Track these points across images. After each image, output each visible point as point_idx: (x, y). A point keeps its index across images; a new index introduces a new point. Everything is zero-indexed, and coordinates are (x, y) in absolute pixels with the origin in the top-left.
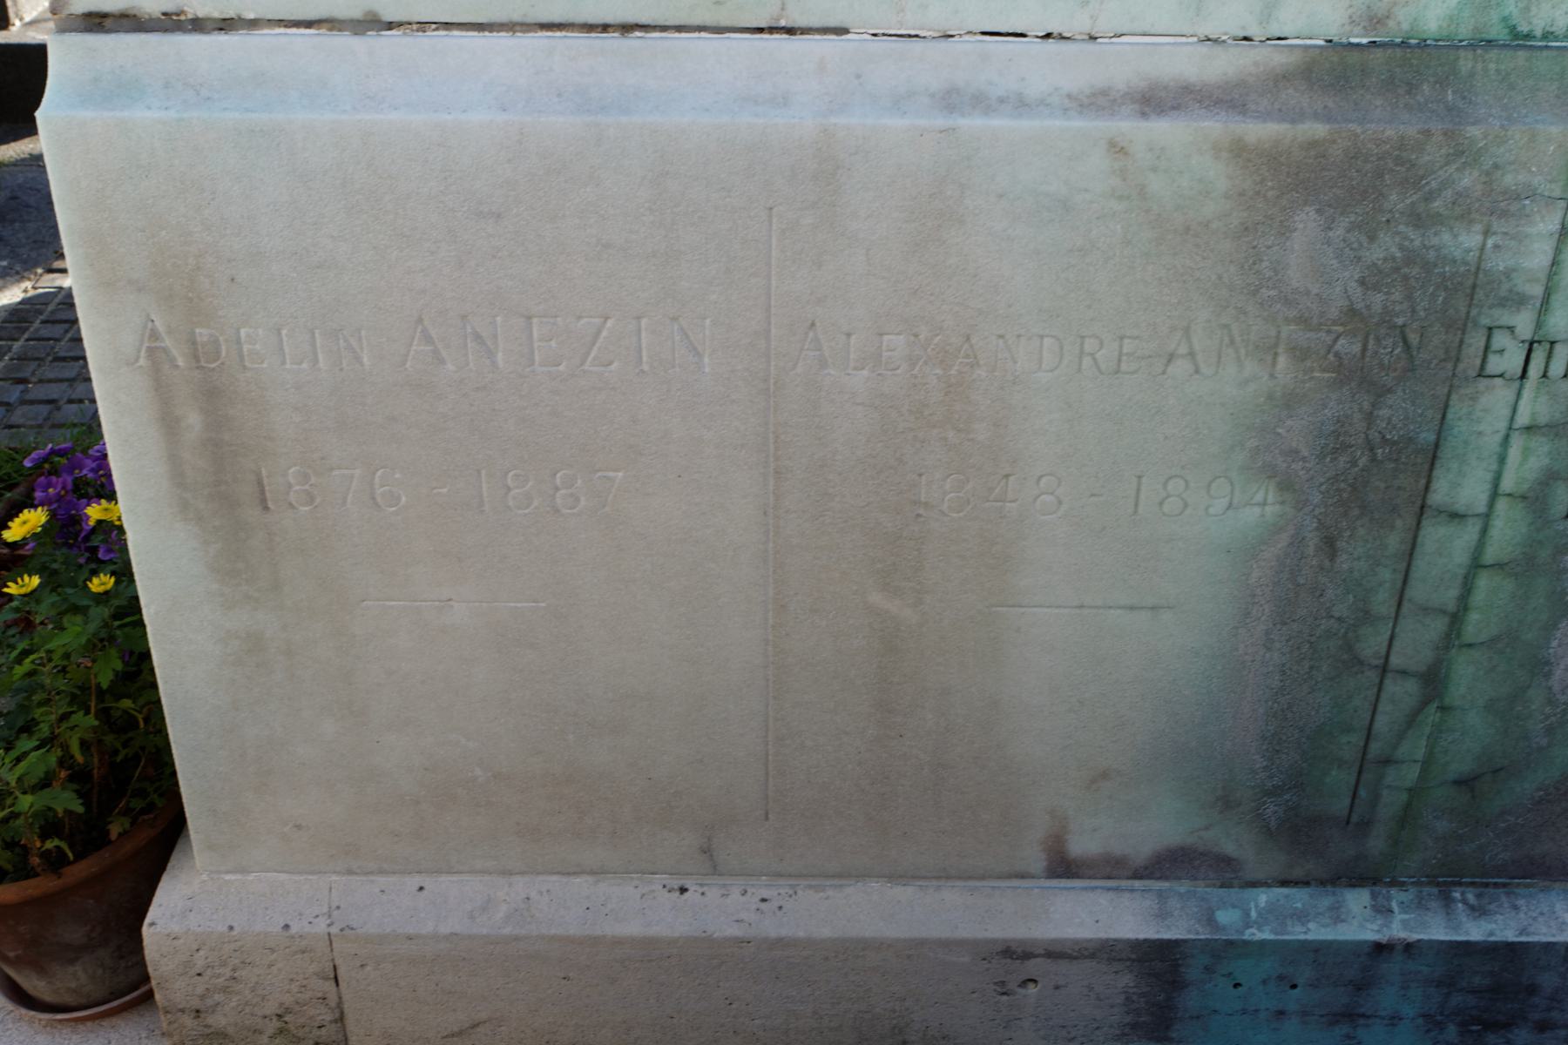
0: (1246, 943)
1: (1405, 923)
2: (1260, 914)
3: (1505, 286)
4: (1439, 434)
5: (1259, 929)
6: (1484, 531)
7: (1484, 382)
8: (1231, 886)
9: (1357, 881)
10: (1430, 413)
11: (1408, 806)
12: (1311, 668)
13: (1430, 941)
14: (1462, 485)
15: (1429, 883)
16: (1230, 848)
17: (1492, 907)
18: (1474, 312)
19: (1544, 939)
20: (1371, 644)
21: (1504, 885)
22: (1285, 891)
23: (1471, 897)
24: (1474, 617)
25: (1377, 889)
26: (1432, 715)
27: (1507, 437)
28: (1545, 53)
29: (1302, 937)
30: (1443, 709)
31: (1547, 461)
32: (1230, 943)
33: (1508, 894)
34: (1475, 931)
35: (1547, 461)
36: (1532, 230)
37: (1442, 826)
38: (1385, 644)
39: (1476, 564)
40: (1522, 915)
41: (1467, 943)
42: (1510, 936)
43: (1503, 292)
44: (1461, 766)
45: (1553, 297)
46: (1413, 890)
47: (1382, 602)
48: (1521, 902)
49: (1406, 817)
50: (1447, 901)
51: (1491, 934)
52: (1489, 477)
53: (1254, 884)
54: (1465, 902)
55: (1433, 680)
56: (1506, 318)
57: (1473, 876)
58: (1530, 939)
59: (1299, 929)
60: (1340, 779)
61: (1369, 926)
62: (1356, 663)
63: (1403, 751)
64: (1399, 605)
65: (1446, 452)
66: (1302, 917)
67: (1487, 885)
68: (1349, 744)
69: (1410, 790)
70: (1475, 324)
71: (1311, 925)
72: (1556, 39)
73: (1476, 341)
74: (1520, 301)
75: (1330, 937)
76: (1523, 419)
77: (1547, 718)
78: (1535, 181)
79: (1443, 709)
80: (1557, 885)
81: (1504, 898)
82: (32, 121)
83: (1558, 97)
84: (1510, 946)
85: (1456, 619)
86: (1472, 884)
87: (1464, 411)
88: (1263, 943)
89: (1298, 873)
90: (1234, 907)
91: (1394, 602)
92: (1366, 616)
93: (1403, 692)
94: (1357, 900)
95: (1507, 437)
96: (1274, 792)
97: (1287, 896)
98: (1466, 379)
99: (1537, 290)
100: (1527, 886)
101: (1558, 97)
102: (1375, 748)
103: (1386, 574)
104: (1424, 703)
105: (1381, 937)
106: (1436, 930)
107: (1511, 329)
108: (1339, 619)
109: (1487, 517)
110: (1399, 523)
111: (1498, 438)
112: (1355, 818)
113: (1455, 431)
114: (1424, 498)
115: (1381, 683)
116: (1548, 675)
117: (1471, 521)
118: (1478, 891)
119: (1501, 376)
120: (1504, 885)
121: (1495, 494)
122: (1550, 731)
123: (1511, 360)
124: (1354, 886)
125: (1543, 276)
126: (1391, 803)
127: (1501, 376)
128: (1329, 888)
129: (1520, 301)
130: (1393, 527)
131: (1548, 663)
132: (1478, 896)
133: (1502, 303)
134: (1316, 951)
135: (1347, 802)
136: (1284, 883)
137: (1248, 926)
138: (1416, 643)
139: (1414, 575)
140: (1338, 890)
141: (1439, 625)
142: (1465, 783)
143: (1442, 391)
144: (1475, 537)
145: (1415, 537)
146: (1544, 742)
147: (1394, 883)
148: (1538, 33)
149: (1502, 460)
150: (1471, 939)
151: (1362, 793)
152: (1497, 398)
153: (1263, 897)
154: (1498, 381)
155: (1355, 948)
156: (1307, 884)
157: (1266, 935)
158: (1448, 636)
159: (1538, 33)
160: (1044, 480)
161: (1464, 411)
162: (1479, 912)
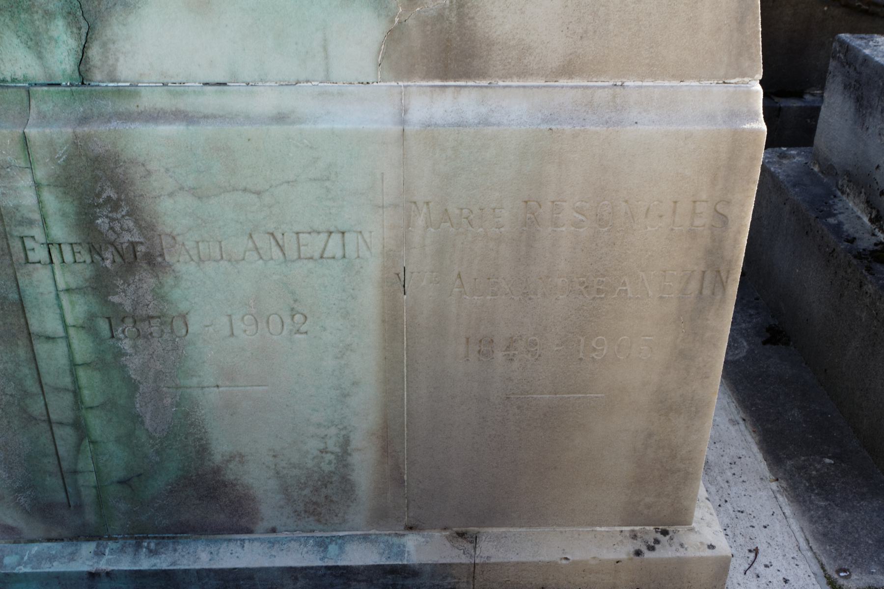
0: (16, 574)
1: (108, 562)
2: (29, 558)
3: (18, 215)
4: (19, 294)
5: (25, 567)
6: (69, 346)
7: (30, 267)
8: (20, 543)
9: (90, 538)
10: (8, 283)
11: (98, 496)
12: (9, 422)
13: (119, 571)
14: (45, 320)
15: (131, 538)
16: (10, 522)
17: (162, 550)
18: (8, 229)
19: (182, 567)
20: (37, 408)
21: (173, 538)
22: (49, 544)
23: (152, 545)
24: (86, 393)
25: (101, 542)
26: (86, 445)
27: (58, 295)
28: (10, 90)
29: (47, 570)
30: (92, 442)
31: (86, 308)
32: (7, 575)
33: (174, 543)
34: (146, 564)
35: (86, 308)
36: (20, 185)
37: (123, 506)
38: (44, 408)
39: (73, 365)
40: (177, 554)
41: (140, 571)
42: (165, 566)
43: (18, 217)
44: (119, 473)
45: (47, 220)
46: (121, 542)
47: (31, 385)
48: (180, 547)
49: (100, 502)
50: (138, 546)
51: (155, 565)
52: (58, 317)
53: (32, 541)
54: (148, 548)
55: (79, 427)
56: (27, 232)
57: (153, 533)
58: (175, 568)
59: (48, 565)
60: (53, 482)
61: (88, 563)
62: (32, 419)
63: (81, 466)
64: (42, 387)
65: (28, 305)
66: (51, 559)
67: (163, 538)
68: (49, 463)
69: (95, 487)
70: (12, 236)
71: (55, 564)
72: (19, 82)
73: (16, 245)
74: (31, 223)
75: (62, 570)
76: (62, 285)
77: (153, 446)
78: (8, 158)
79: (92, 442)
80: (203, 537)
81: (171, 545)
82: (812, 142)
83: (20, 113)
84: (165, 572)
85: (76, 392)
86: (155, 538)
87: (27, 282)
88: (25, 574)
89: (54, 534)
90: (17, 554)
91: (37, 385)
92: (26, 394)
93: (65, 436)
94: (87, 548)
95: (58, 295)
96: (19, 490)
97: (49, 548)
98: (20, 264)
99: (37, 216)
100: (186, 538)
101: (20, 113)
102: (65, 465)
103: (26, 370)
104: (81, 439)
105: (92, 569)
106: (125, 564)
107: (33, 237)
108: (11, 395)
109: (67, 337)
110: (20, 343)
111: (53, 295)
112: (72, 503)
113: (27, 292)
114: (28, 329)
115: (51, 429)
116: (142, 423)
117: (59, 341)
118: (158, 541)
119: (39, 262)
120: (173, 538)
121: (66, 327)
122: (157, 452)
123: (40, 254)
124: (89, 541)
125: (36, 208)
126: (88, 495)
127: (39, 262)
128: (75, 542)
129: (31, 223)
130: (18, 345)
131: (139, 416)
132: (157, 545)
133: (21, 223)
134: (58, 577)
135: (63, 495)
136: (49, 540)
137: (19, 565)
138: (61, 407)
139: (42, 371)
140: (79, 543)
141: (68, 398)
142: (123, 482)
143: (10, 271)
144: (66, 349)
145: (33, 350)
146: (158, 459)
147: (110, 538)
148: (9, 79)
149: (61, 307)
150: (142, 568)
151: (69, 489)
152: (42, 275)
153: (35, 548)
154: (38, 265)
155: (79, 575)
156: (62, 540)
157: (28, 570)
158: (76, 402)
159: (9, 79)
160: (246, 318)
161: (27, 282)
162: (152, 553)
